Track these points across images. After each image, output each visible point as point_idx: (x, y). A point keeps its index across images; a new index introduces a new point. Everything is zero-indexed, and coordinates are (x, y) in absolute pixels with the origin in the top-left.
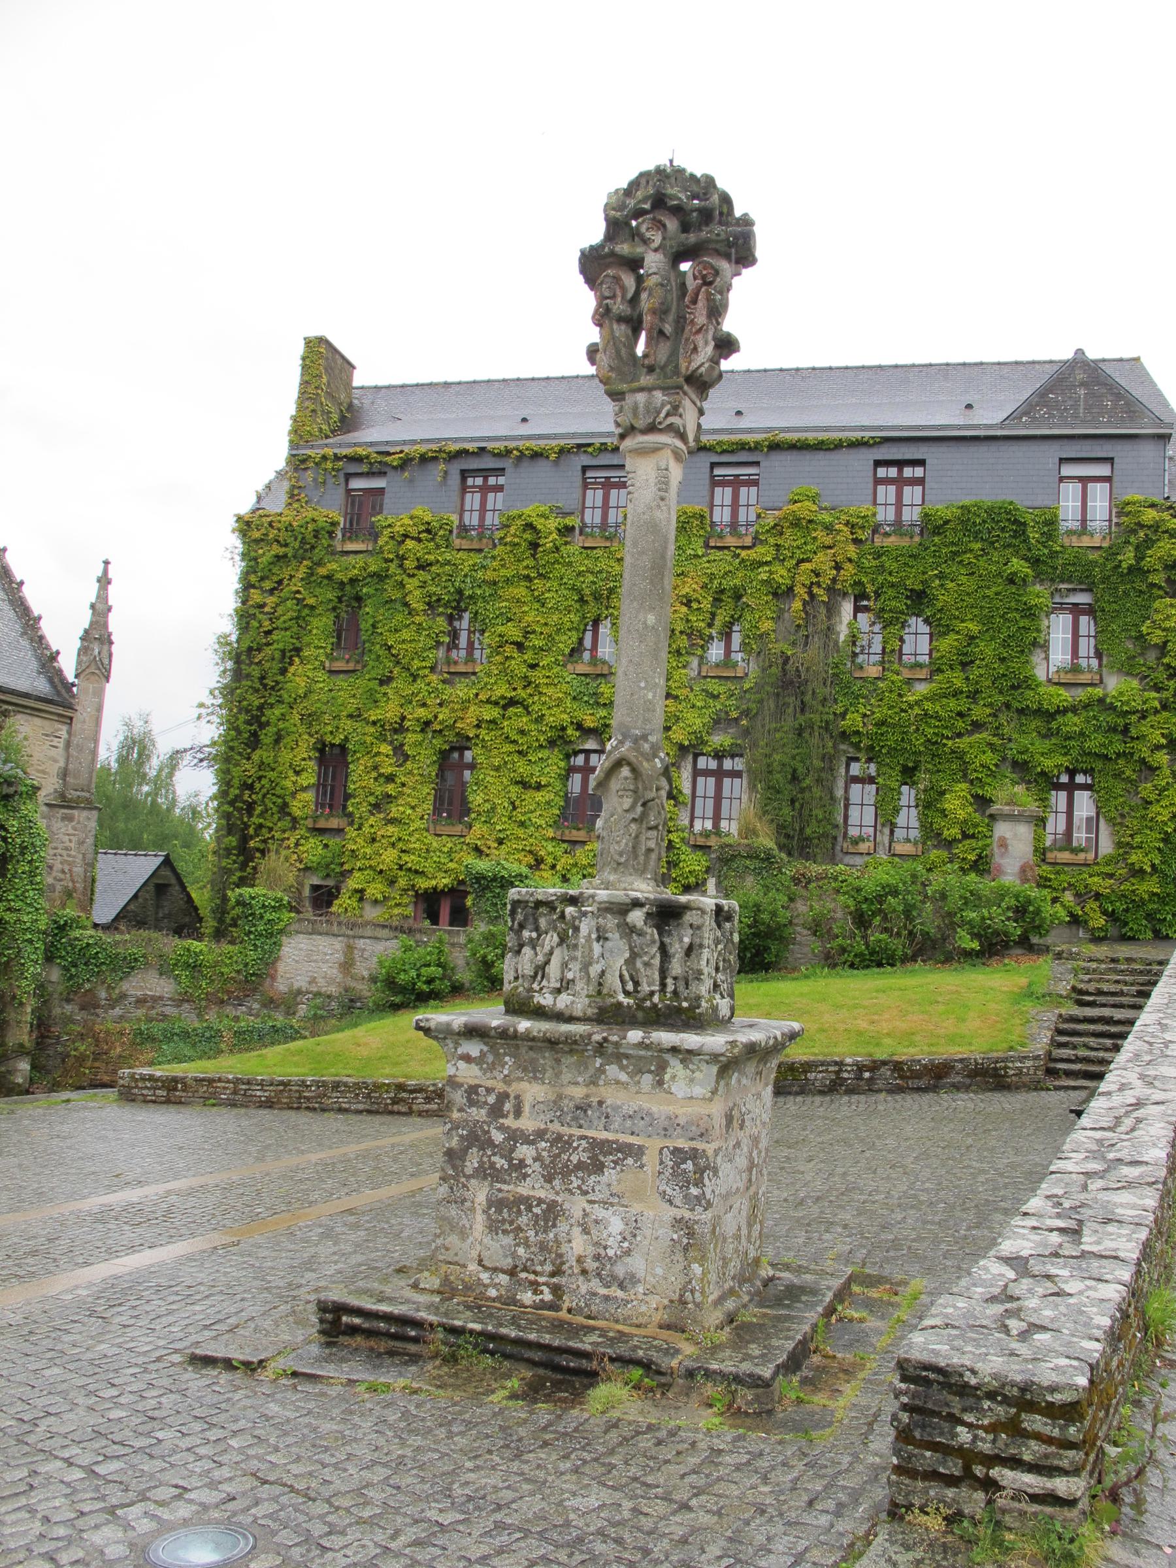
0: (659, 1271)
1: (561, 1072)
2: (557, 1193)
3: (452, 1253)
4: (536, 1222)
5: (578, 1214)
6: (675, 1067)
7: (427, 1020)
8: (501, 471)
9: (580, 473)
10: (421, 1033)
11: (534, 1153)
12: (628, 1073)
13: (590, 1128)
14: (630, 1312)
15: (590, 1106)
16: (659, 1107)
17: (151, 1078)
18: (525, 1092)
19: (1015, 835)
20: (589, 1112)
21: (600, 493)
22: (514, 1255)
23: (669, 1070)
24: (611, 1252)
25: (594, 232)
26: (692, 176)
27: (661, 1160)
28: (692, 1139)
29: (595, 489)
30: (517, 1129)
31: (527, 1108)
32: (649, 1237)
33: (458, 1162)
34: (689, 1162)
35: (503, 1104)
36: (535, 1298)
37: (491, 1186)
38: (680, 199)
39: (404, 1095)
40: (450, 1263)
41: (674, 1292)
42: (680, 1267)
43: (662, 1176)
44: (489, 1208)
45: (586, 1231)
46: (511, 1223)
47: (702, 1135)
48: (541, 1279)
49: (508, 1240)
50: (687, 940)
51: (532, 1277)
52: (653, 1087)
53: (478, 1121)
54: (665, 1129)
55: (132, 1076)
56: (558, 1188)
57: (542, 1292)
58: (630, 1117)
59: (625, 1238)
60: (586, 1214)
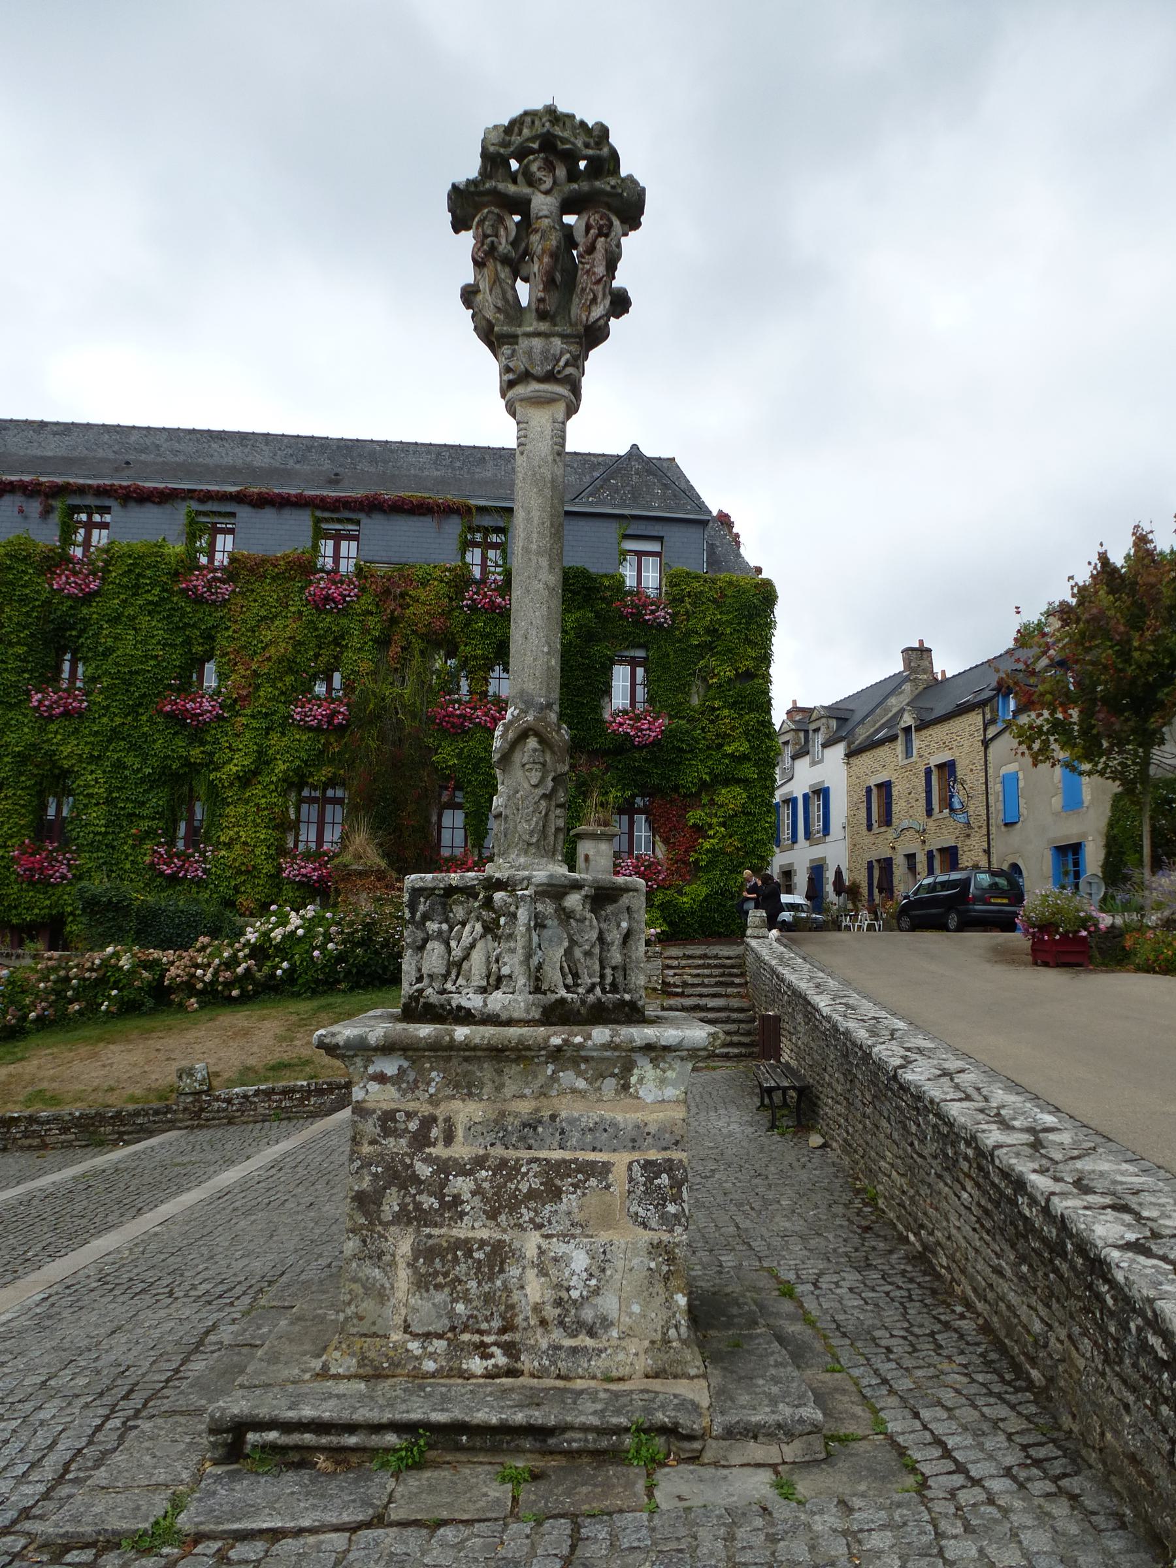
0: (636, 1309)
1: (503, 1085)
2: (504, 1231)
3: (366, 1323)
4: (479, 1269)
5: (531, 1252)
6: (645, 1069)
7: (333, 1035)
8: (105, 510)
10: (322, 1051)
11: (472, 1185)
12: (586, 1079)
13: (540, 1148)
14: (607, 1364)
15: (540, 1122)
16: (624, 1116)
18: (457, 1112)
19: (598, 852)
20: (540, 1129)
22: (452, 1314)
23: (635, 1071)
24: (575, 1294)
25: (469, 168)
26: (583, 124)
27: (630, 1176)
28: (665, 1149)
30: (449, 1159)
31: (460, 1133)
32: (620, 1269)
33: (373, 1207)
34: (664, 1176)
35: (429, 1131)
36: (485, 1363)
37: (418, 1231)
38: (573, 144)
39: (35, 1127)
40: (365, 1335)
41: (656, 1331)
42: (660, 1300)
43: (633, 1196)
44: (416, 1259)
45: (543, 1272)
46: (446, 1275)
47: (677, 1143)
48: (488, 1339)
49: (441, 1297)
50: (624, 925)
51: (476, 1338)
52: (617, 1092)
53: (398, 1154)
54: (634, 1140)
56: (504, 1224)
57: (492, 1356)
58: (590, 1130)
59: (591, 1275)
60: (541, 1252)
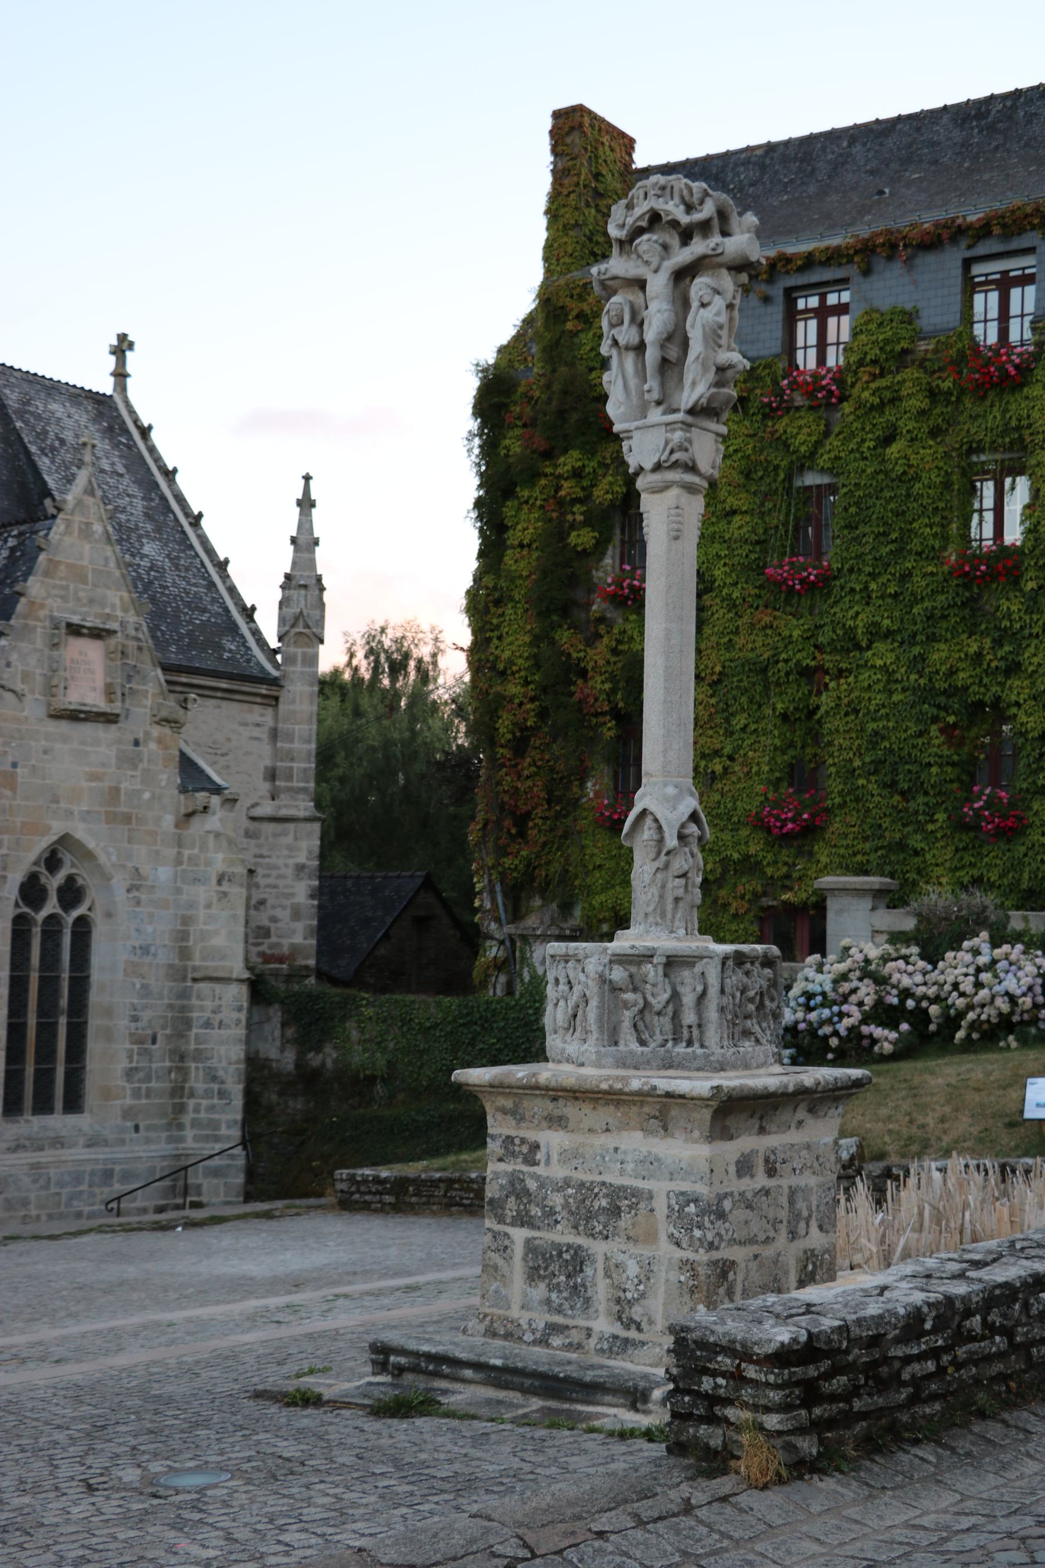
9: (958, 272)
17: (377, 1180)
21: (994, 297)
29: (986, 292)
33: (500, 1211)
34: (692, 1205)
54: (671, 1174)
55: (352, 1179)
